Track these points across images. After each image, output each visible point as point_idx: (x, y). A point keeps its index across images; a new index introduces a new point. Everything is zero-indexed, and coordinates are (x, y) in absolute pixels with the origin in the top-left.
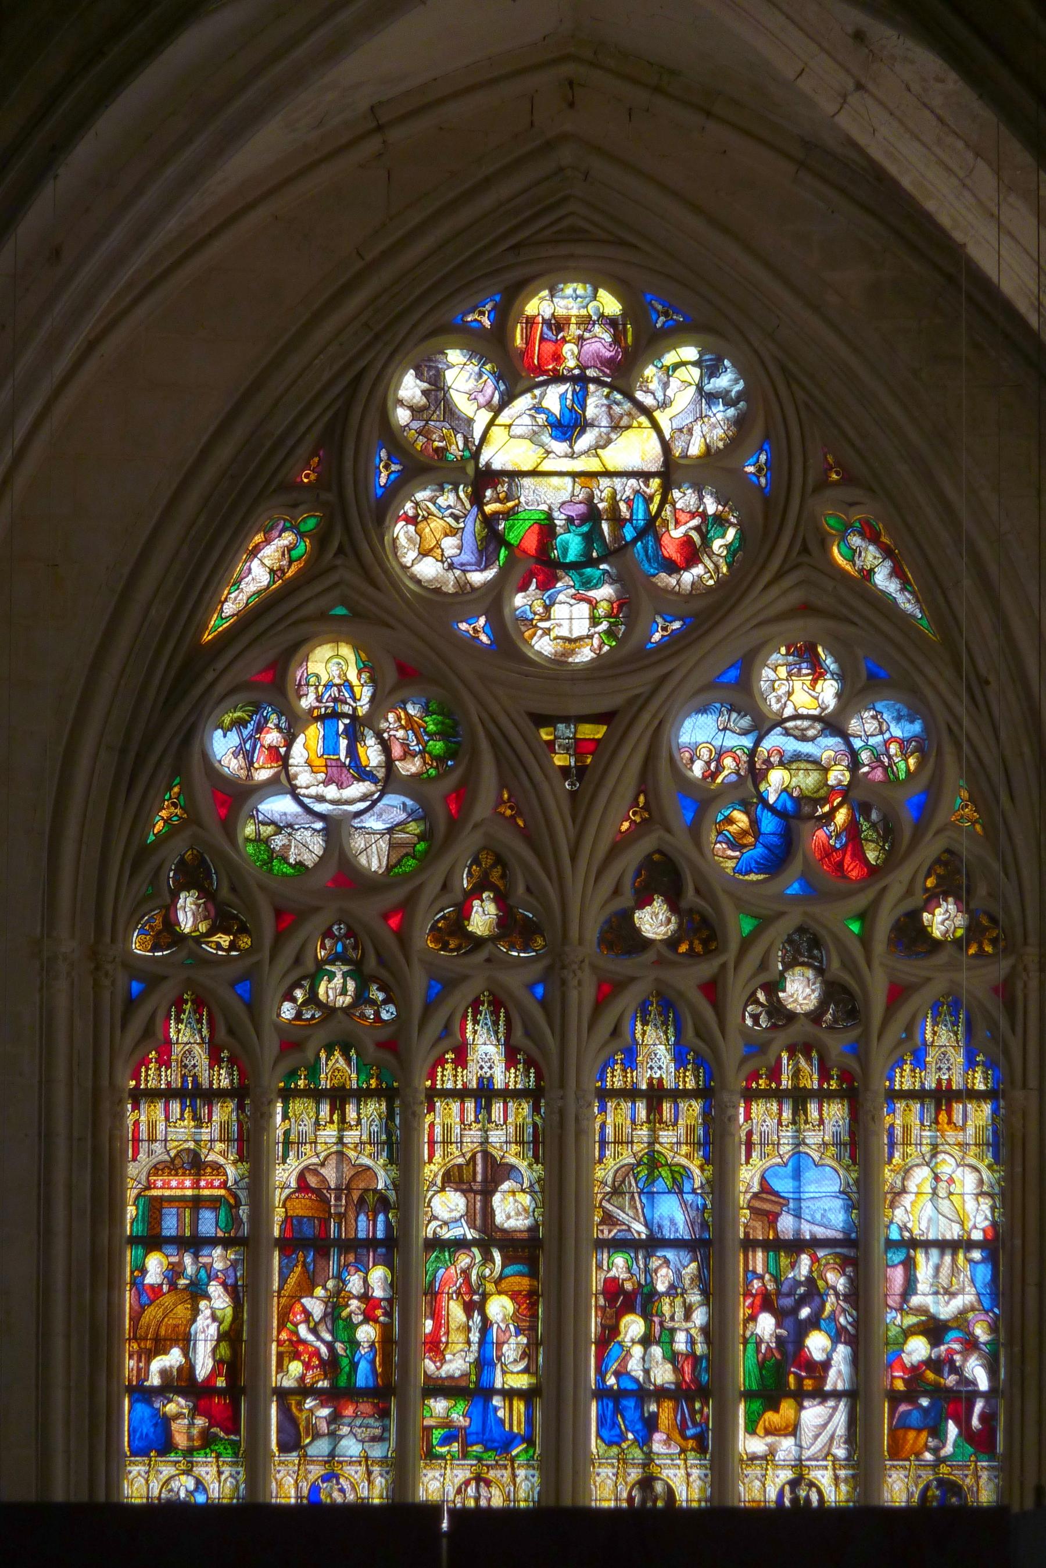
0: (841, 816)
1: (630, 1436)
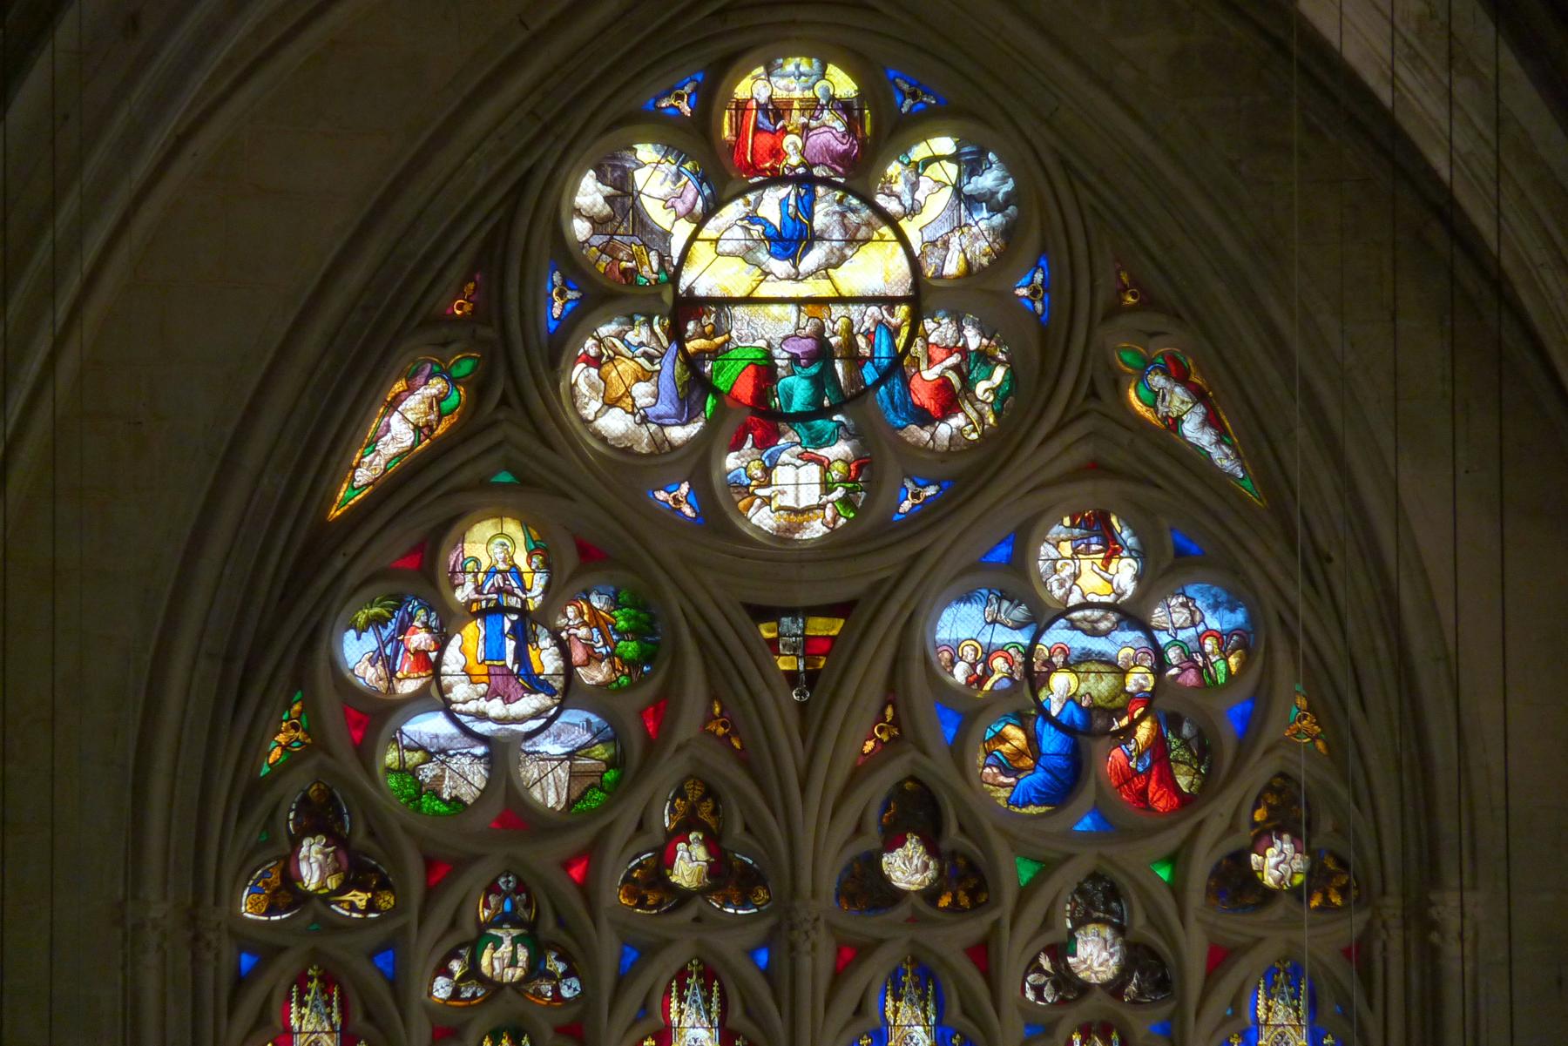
0: (1144, 731)
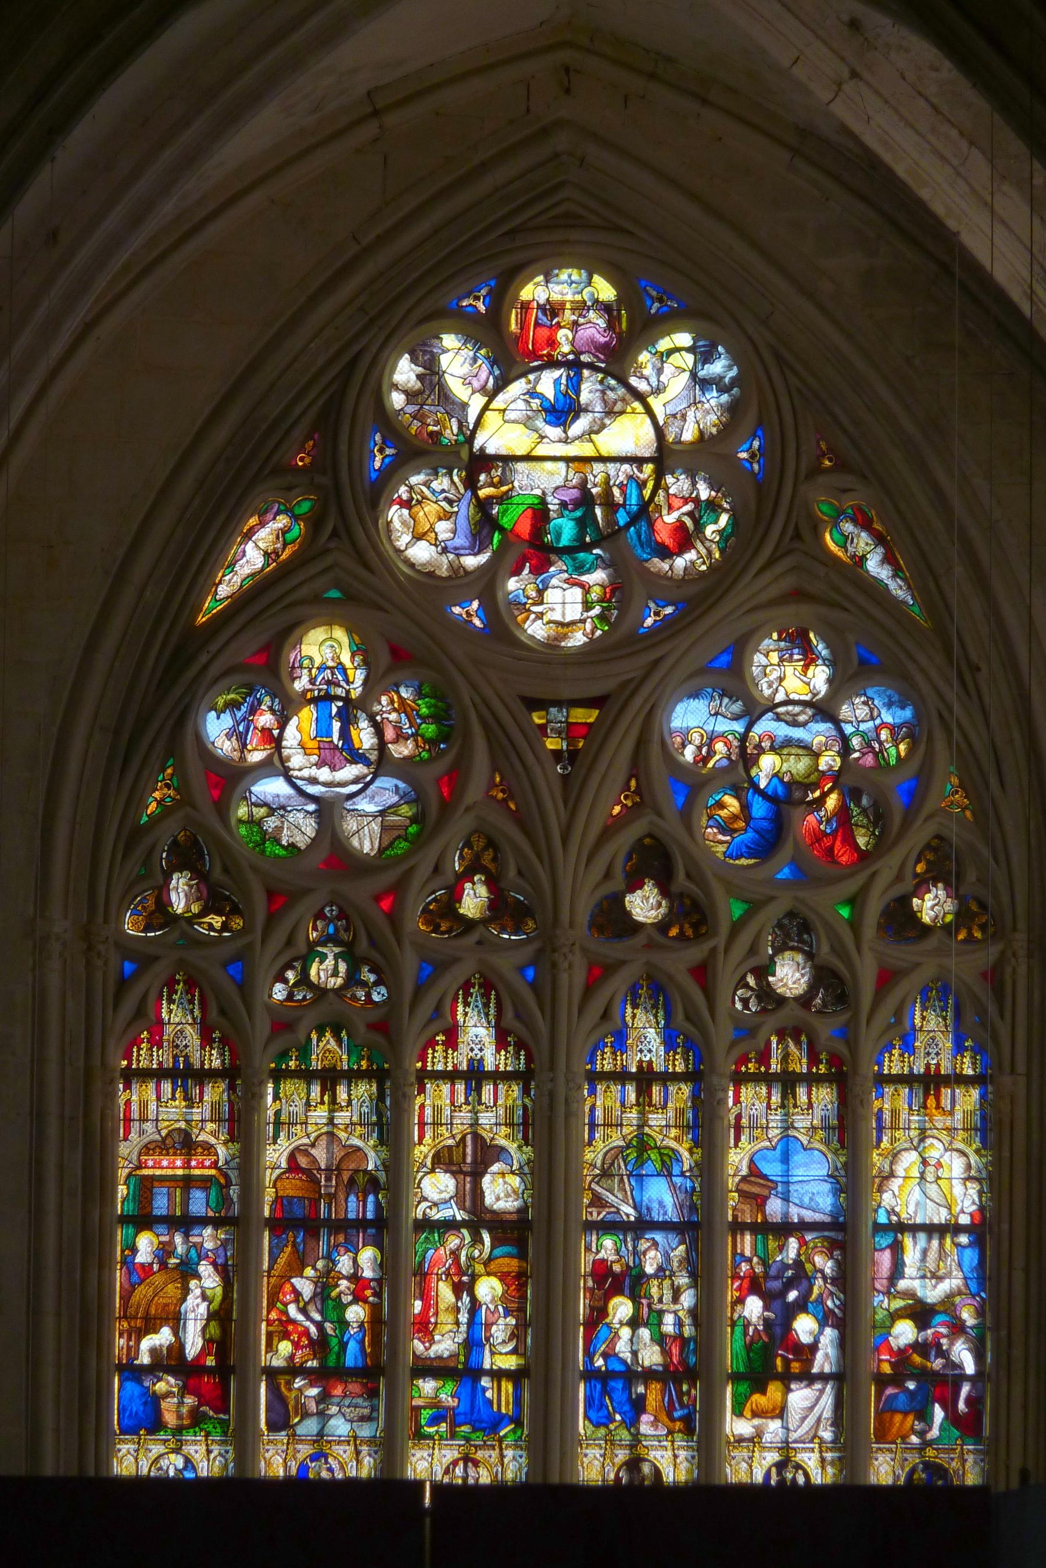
0: (832, 801)
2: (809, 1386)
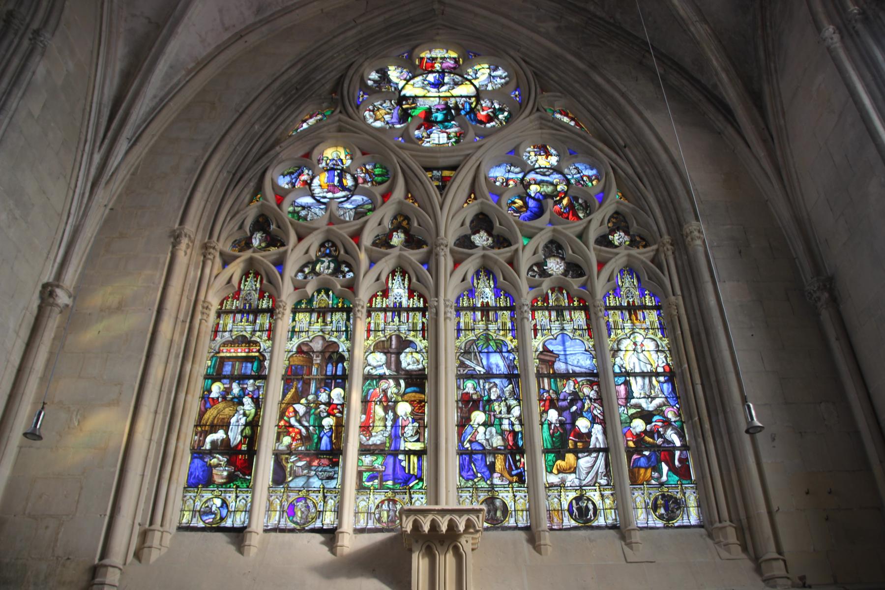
0: (565, 202)
1: (479, 475)
2: (589, 455)
